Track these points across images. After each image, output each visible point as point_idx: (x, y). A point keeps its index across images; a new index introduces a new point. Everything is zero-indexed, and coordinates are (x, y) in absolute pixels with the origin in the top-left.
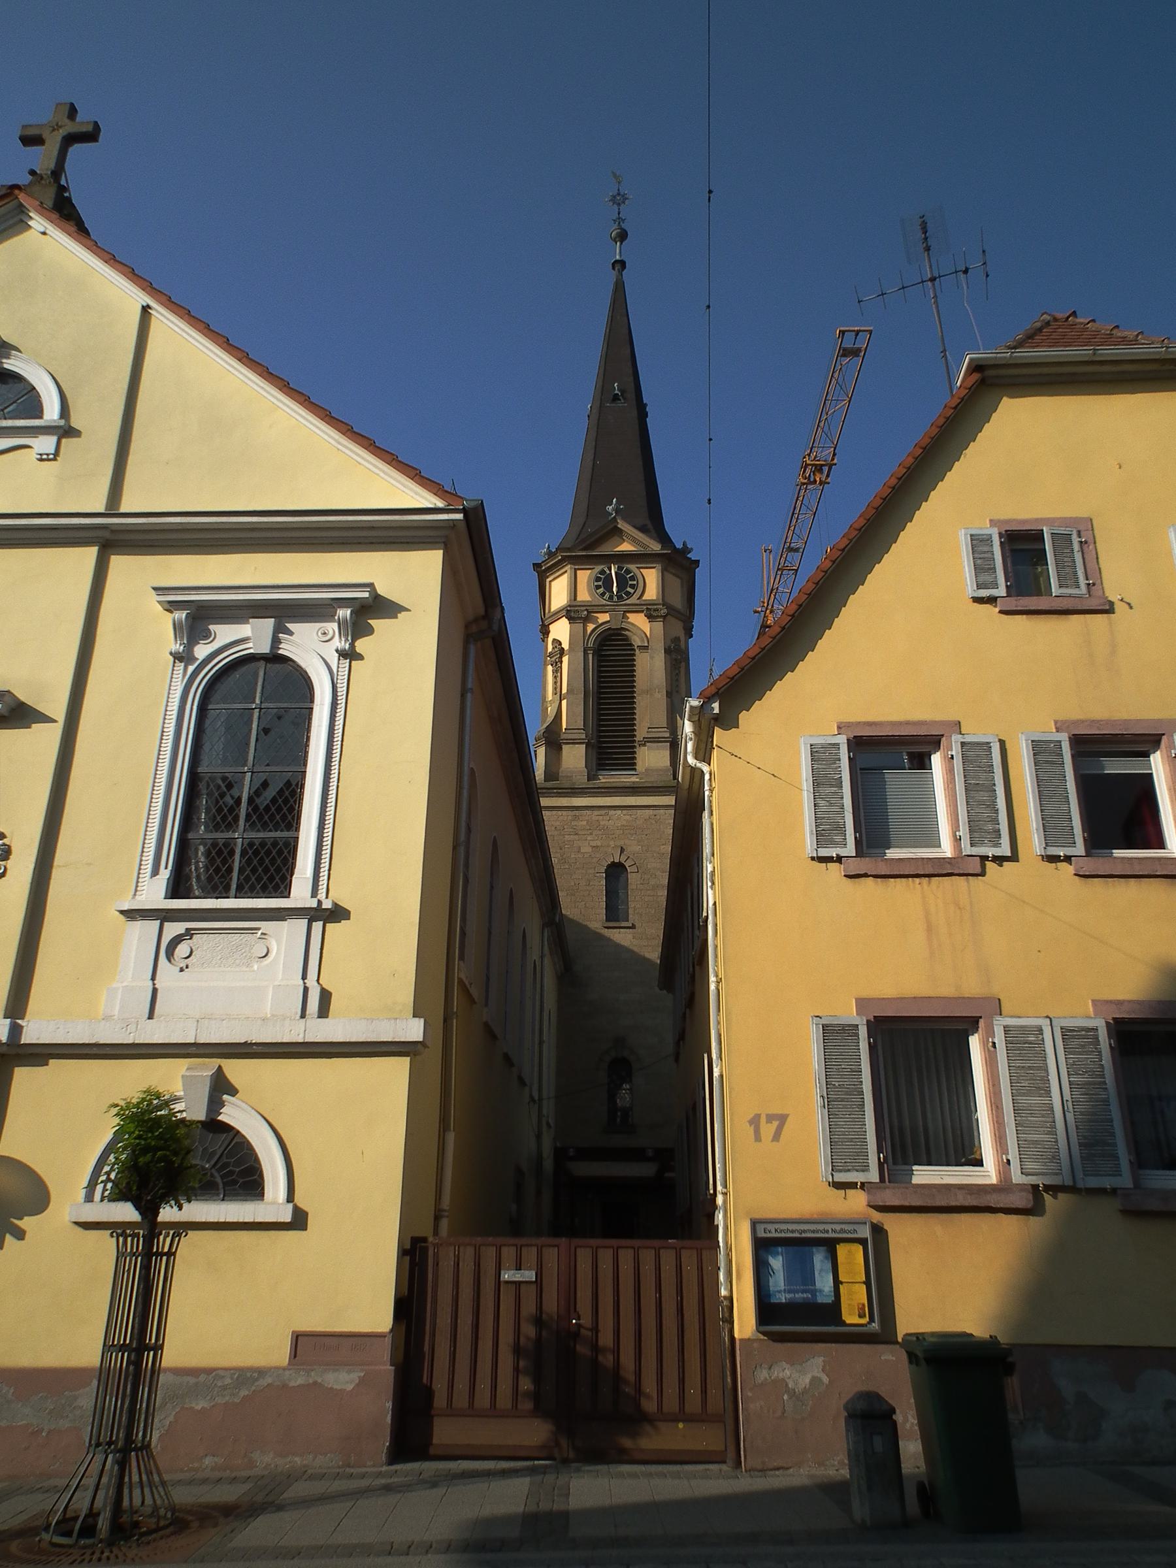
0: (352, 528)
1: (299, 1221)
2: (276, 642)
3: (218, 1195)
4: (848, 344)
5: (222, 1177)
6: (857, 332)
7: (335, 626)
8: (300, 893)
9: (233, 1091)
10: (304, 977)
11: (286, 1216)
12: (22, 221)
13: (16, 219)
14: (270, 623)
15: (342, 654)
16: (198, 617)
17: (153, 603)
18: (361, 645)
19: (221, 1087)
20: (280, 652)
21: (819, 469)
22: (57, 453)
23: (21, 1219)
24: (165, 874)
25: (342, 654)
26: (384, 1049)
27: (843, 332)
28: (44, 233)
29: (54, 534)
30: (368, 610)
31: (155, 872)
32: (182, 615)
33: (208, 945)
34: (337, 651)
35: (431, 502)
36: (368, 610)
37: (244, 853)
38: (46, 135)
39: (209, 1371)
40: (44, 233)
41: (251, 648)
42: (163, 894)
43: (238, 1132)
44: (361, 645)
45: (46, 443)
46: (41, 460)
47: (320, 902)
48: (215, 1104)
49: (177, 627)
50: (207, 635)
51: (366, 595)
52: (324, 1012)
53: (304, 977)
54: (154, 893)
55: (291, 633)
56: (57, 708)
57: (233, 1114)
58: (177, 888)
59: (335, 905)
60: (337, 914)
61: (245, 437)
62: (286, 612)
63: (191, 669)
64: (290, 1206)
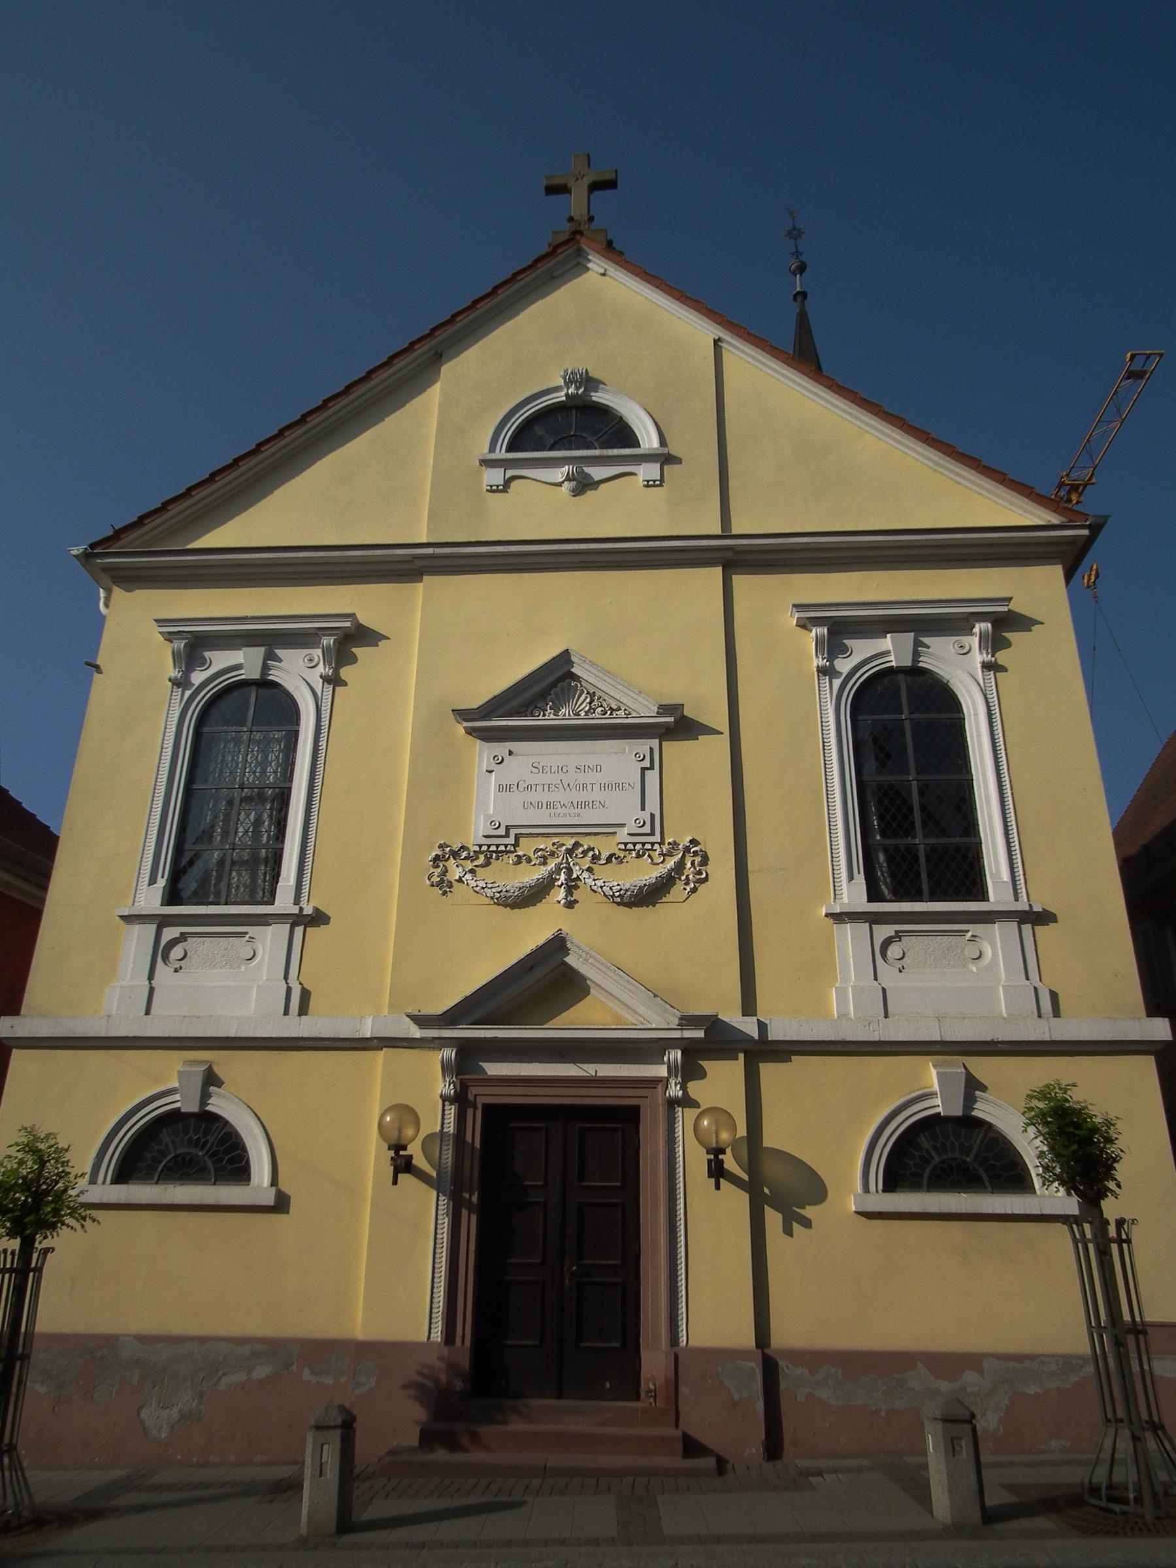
0: (900, 547)
1: (281, 1204)
2: (265, 668)
3: (210, 1180)
4: (1137, 366)
5: (214, 1163)
6: (1149, 356)
7: (319, 652)
8: (284, 902)
9: (984, 1088)
10: (286, 978)
11: (269, 1199)
12: (579, 264)
13: (574, 262)
14: (260, 652)
15: (326, 679)
16: (194, 646)
17: (156, 634)
18: (345, 673)
19: (973, 1086)
20: (921, 664)
21: (1074, 488)
22: (662, 480)
23: (804, 1208)
24: (161, 883)
25: (326, 679)
26: (1091, 1048)
27: (1133, 357)
28: (604, 275)
29: (681, 556)
30: (1006, 624)
31: (152, 881)
32: (181, 644)
33: (919, 947)
34: (321, 677)
35: (1043, 520)
36: (1006, 624)
37: (928, 858)
38: (571, 184)
39: (1032, 1357)
40: (604, 275)
41: (244, 675)
42: (159, 902)
43: (227, 1122)
44: (345, 673)
45: (650, 471)
46: (648, 486)
47: (301, 909)
48: (970, 1100)
49: (176, 656)
50: (203, 663)
51: (349, 624)
52: (303, 1010)
53: (286, 978)
54: (151, 899)
55: (280, 660)
56: (721, 721)
57: (218, 1105)
58: (173, 896)
59: (316, 910)
60: (319, 919)
61: (835, 458)
62: (273, 639)
63: (188, 693)
64: (273, 1190)
